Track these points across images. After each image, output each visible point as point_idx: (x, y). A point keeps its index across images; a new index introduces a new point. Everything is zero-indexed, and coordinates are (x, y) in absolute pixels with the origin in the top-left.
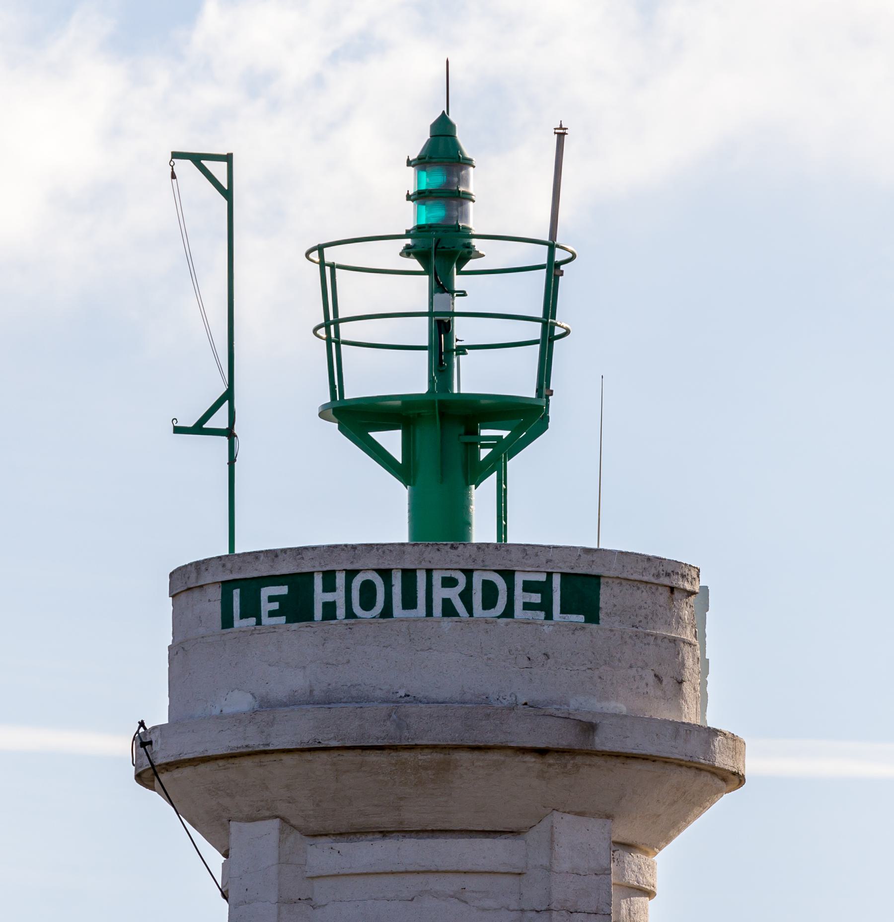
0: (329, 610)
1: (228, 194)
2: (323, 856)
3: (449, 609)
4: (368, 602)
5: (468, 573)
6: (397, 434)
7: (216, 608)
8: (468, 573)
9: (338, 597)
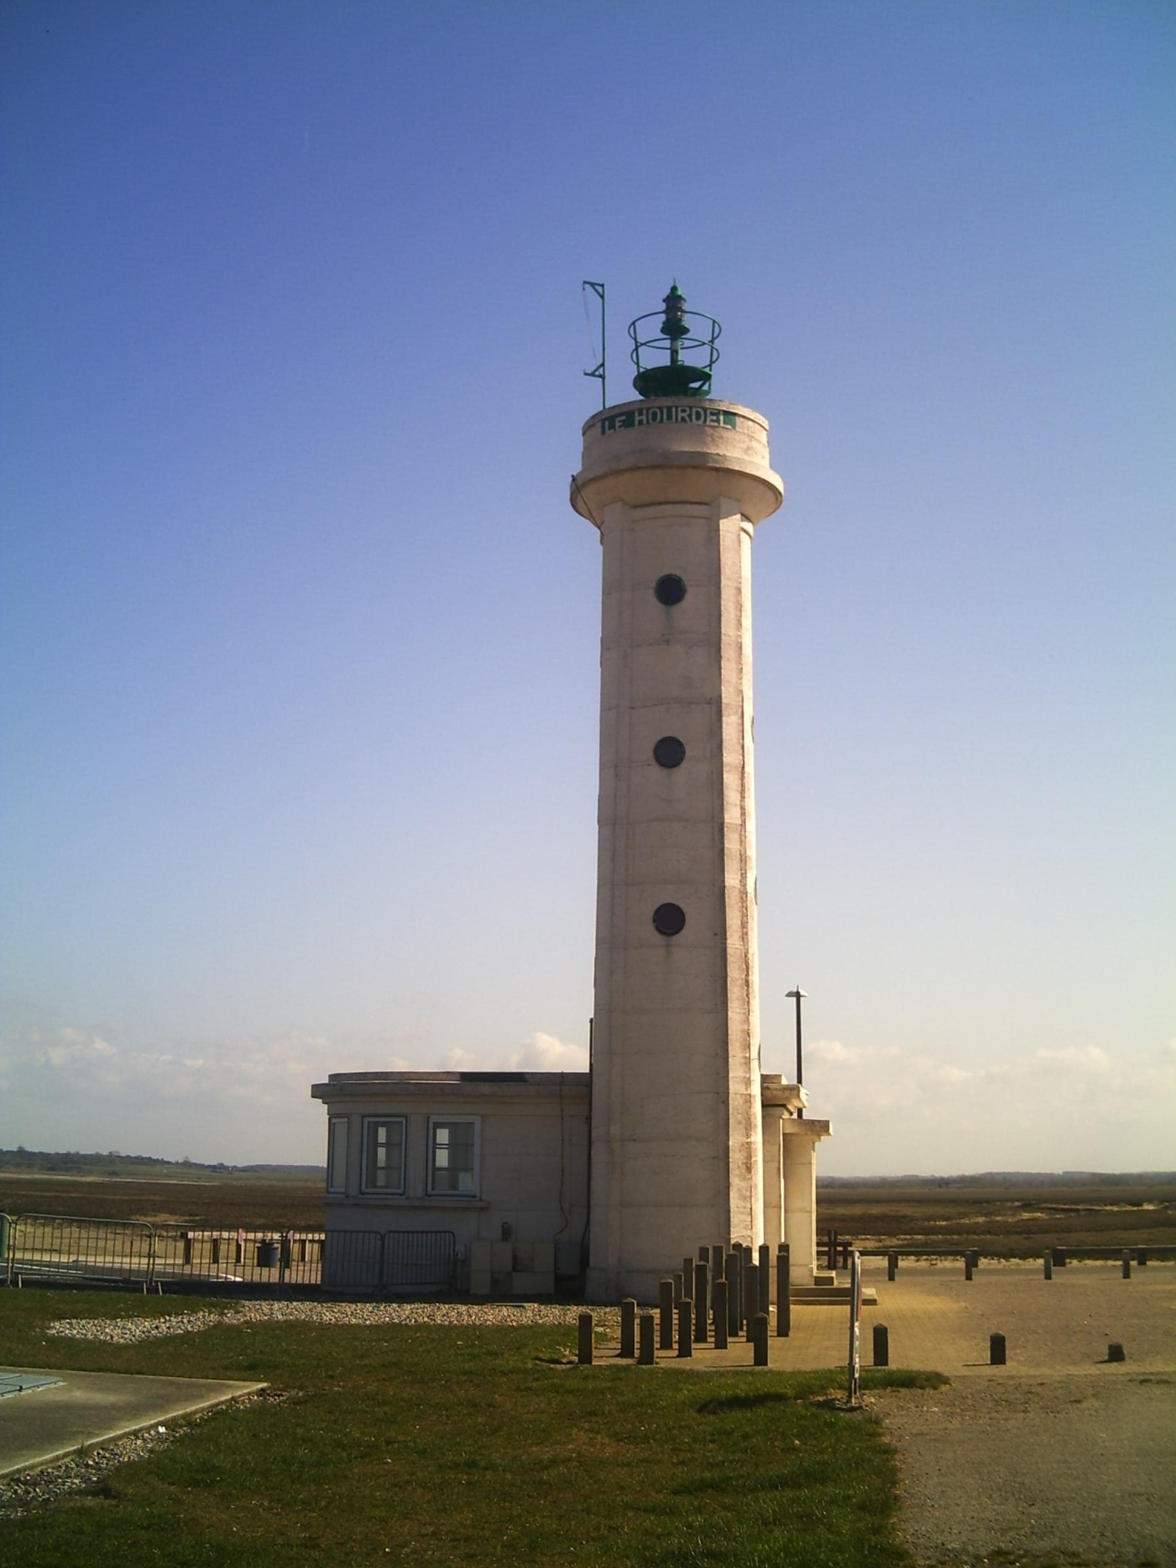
0: (641, 422)
1: (602, 297)
2: (638, 514)
3: (683, 419)
4: (654, 419)
5: (691, 408)
6: (658, 1311)
7: (600, 429)
8: (691, 408)
9: (644, 418)
